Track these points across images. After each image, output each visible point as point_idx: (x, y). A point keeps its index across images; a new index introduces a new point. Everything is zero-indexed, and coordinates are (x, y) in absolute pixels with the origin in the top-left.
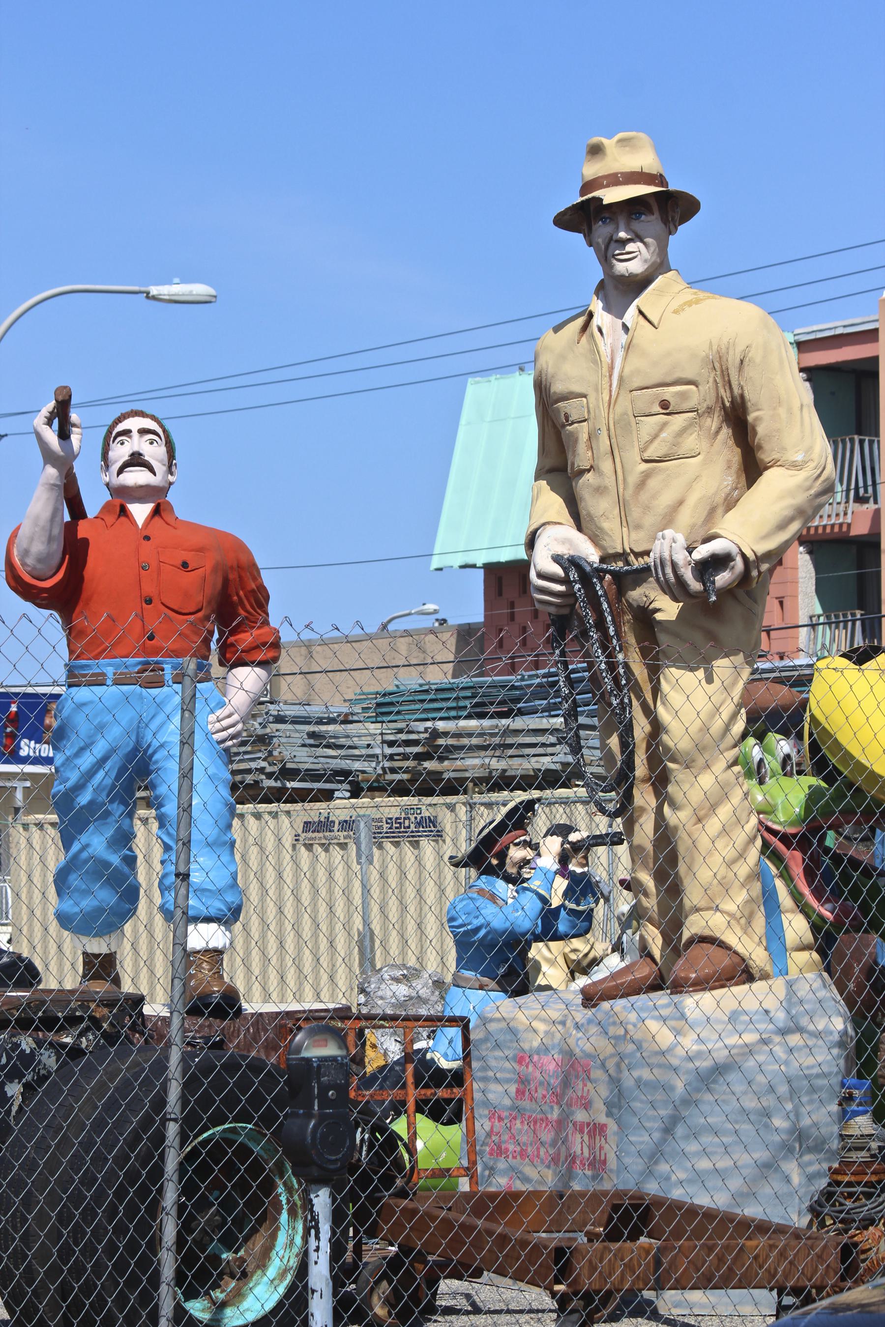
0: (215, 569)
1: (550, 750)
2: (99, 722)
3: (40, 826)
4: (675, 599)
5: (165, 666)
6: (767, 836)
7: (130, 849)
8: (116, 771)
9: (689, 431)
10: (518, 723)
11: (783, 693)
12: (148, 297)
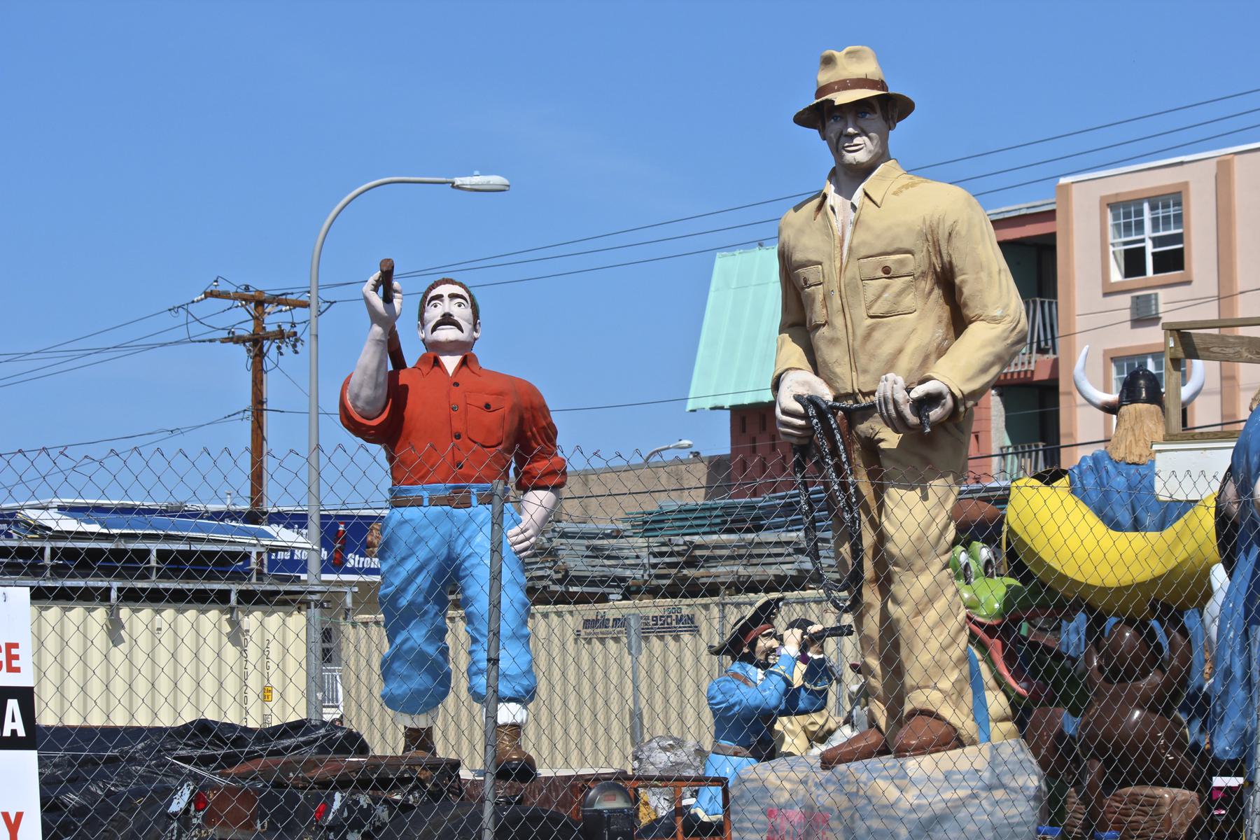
0: (512, 410)
3: (366, 624)
4: (897, 431)
6: (975, 628)
10: (765, 536)
11: (987, 508)
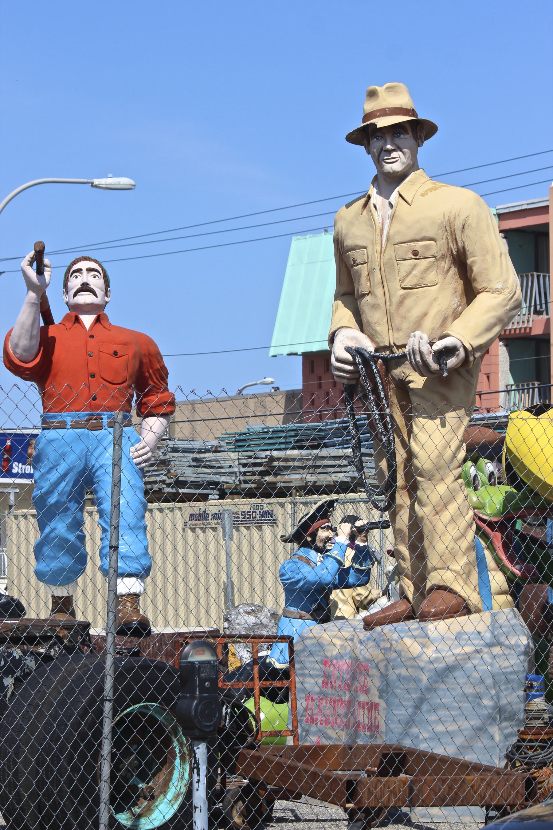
0: (134, 356)
1: (344, 469)
2: (62, 452)
3: (25, 516)
4: (422, 375)
5: (103, 417)
6: (479, 523)
7: (81, 531)
8: (72, 482)
9: (431, 270)
10: (324, 452)
11: (489, 434)
12: (92, 186)
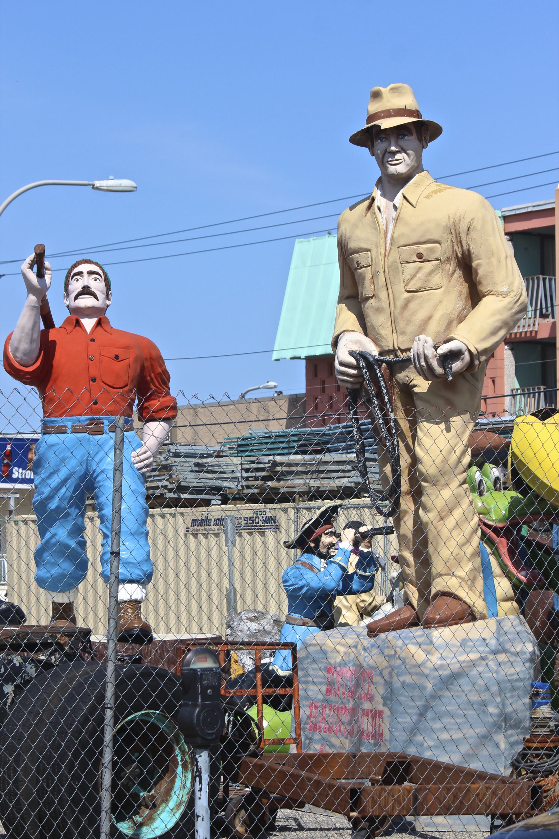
0: (136, 360)
1: (347, 474)
2: (63, 457)
3: (25, 522)
4: (427, 379)
5: (104, 421)
6: (485, 528)
7: (82, 537)
8: (73, 488)
9: (435, 273)
10: (327, 457)
11: (495, 438)
12: (93, 188)
